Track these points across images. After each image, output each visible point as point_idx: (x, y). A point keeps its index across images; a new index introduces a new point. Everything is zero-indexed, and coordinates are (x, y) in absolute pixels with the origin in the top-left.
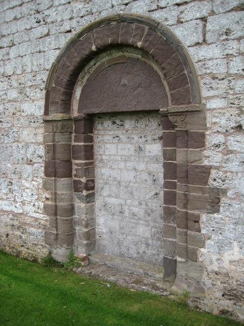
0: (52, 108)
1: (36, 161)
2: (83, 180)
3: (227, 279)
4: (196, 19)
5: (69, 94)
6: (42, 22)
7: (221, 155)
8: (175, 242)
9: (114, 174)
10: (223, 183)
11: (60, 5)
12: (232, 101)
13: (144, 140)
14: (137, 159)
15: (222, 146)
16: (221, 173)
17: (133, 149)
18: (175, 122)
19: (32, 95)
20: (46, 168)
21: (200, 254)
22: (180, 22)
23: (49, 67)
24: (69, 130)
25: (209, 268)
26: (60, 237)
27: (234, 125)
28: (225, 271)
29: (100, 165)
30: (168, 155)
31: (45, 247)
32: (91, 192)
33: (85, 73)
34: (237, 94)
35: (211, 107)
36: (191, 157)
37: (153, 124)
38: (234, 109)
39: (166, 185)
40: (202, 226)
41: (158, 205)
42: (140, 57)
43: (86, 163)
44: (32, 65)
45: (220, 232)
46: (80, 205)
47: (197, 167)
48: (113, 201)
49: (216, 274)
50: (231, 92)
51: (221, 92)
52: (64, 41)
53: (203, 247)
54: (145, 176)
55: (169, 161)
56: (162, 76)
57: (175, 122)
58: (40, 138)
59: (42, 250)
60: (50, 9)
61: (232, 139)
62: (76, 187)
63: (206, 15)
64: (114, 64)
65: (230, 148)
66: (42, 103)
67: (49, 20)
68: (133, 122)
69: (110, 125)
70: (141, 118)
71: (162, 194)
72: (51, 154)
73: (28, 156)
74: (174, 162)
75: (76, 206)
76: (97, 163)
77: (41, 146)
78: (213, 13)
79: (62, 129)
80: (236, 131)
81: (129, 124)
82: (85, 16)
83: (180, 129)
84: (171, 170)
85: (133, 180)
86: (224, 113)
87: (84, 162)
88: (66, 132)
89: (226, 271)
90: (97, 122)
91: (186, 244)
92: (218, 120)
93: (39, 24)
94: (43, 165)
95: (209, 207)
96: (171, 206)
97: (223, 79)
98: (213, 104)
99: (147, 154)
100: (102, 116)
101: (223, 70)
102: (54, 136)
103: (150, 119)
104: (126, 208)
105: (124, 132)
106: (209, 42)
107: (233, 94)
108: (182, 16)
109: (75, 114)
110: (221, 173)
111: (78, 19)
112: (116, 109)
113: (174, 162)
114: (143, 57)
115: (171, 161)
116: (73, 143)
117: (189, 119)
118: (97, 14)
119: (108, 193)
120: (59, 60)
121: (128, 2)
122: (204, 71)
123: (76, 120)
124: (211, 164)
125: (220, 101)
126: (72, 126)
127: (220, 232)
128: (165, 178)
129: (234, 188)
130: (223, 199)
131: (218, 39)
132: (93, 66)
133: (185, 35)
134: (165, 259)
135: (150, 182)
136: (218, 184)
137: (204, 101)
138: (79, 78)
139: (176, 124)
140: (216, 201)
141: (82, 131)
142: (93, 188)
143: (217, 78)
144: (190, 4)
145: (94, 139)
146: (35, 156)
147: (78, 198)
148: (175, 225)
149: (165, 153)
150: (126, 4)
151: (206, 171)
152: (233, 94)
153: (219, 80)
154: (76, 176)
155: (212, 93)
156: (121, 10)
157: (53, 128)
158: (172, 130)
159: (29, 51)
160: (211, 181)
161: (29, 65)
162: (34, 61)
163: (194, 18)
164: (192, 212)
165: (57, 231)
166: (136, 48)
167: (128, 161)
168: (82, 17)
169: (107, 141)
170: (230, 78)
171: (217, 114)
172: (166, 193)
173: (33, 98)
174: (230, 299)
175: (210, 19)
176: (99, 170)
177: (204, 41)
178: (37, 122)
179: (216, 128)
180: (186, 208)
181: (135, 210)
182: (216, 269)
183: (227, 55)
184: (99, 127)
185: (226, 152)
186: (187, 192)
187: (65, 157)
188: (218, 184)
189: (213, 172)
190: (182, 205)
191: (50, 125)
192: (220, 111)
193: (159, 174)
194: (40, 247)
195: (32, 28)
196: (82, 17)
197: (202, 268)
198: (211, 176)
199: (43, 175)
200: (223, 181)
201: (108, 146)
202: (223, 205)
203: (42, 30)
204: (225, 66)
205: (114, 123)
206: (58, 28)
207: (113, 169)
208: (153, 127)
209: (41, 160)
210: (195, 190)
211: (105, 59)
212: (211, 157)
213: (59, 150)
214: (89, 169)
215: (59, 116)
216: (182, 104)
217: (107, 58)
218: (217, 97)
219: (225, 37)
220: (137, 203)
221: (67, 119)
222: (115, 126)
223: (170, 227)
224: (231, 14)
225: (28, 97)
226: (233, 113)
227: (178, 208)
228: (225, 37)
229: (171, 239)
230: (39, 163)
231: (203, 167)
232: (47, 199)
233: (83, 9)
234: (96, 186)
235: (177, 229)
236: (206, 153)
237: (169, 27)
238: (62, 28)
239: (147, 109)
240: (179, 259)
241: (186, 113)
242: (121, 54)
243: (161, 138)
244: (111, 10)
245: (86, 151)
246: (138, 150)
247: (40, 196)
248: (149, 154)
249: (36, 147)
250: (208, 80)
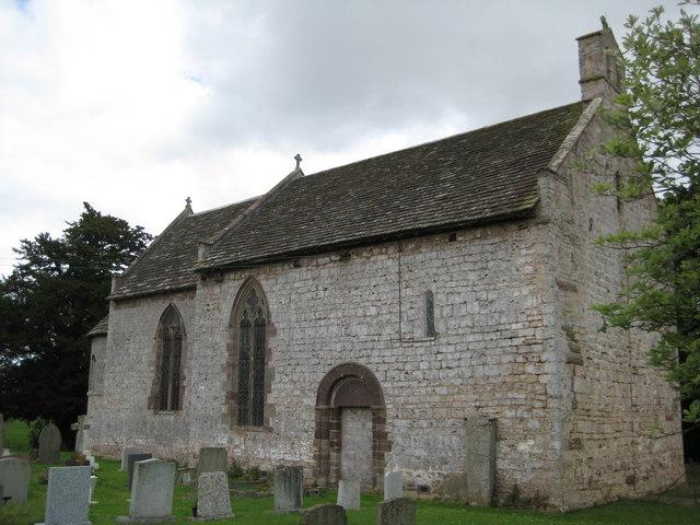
5: (329, 396)
46: (333, 454)
81: (359, 412)
109: (332, 406)
132: (342, 383)
167: (356, 430)
208: (369, 415)
212: (388, 428)
214: (339, 435)
215: (324, 407)
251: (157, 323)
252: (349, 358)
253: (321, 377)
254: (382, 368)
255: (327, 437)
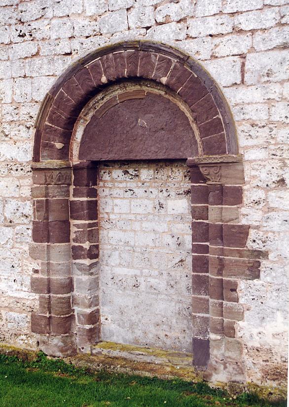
0: (44, 153)
1: (20, 222)
2: (86, 245)
3: (270, 355)
4: (233, 55)
5: (67, 137)
6: (27, 37)
7: (261, 212)
8: (207, 318)
9: (128, 236)
10: (265, 244)
11: (54, 17)
12: (274, 152)
13: (166, 194)
14: (156, 218)
15: (262, 202)
16: (261, 233)
17: (150, 207)
18: (207, 175)
19: (12, 133)
20: (34, 231)
21: (239, 328)
22: (214, 57)
23: (41, 97)
24: (67, 182)
25: (250, 345)
26: (53, 321)
27: (276, 179)
28: (268, 347)
29: (107, 226)
30: (197, 213)
31: (31, 337)
32: (94, 261)
33: (90, 109)
34: (279, 144)
35: (250, 159)
36: (227, 215)
37: (177, 174)
38: (276, 161)
39: (195, 249)
40: (240, 294)
41: (184, 276)
42: (163, 93)
43: (89, 224)
44: (14, 93)
45: (261, 300)
46: (81, 278)
47: (233, 227)
48: (121, 271)
49: (258, 350)
50: (273, 142)
51: (261, 141)
52: (61, 67)
53: (242, 319)
54: (168, 239)
55: (199, 221)
56: (191, 119)
57: (207, 175)
58: (26, 192)
59: (26, 341)
60: (39, 21)
61: (273, 194)
62: (76, 253)
63: (245, 51)
64: (129, 100)
65: (272, 205)
66: (30, 145)
67: (38, 35)
68: (151, 172)
69: (120, 175)
70: (161, 167)
71: (189, 261)
72: (43, 213)
73: (6, 215)
74: (205, 221)
75: (75, 280)
76: (102, 223)
77: (28, 203)
78: (252, 49)
79: (59, 180)
80: (278, 186)
81: (146, 173)
82: (90, 36)
83: (212, 184)
84: (203, 232)
85: (151, 244)
86: (264, 166)
87: (87, 222)
88: (63, 184)
89: (269, 347)
90: (103, 171)
91: (220, 318)
92: (257, 173)
93: (22, 39)
94: (31, 227)
95: (248, 272)
96: (201, 274)
97: (264, 126)
98: (249, 155)
99: (170, 211)
100: (109, 164)
101: (264, 116)
102: (47, 188)
103: (174, 169)
104: (141, 280)
105: (140, 184)
106: (249, 83)
107: (275, 144)
108: (216, 50)
109: (75, 161)
110: (261, 233)
111: (83, 39)
112: (132, 157)
113: (205, 221)
114: (166, 93)
115: (201, 221)
116: (72, 199)
117: (224, 171)
118: (109, 35)
119: (118, 262)
120: (55, 89)
121: (149, 26)
122: (242, 117)
123: (76, 169)
124: (250, 223)
125: (260, 151)
126: (71, 177)
127: (261, 300)
128: (194, 240)
129: (277, 249)
130: (264, 262)
131: (259, 82)
132: (101, 100)
133: (221, 73)
134: (195, 340)
135: (173, 246)
136: (258, 246)
137: (241, 151)
138: (81, 115)
139: (208, 177)
140: (256, 265)
141: (85, 182)
142: (96, 256)
143: (257, 125)
144: (226, 37)
145: (98, 192)
146: (18, 214)
147: (79, 269)
148: (207, 297)
149: (194, 213)
150: (147, 28)
151: (243, 232)
152: (275, 144)
153: (260, 127)
154: (75, 240)
155: (250, 142)
156: (140, 34)
157: (46, 179)
158: (202, 183)
159: (9, 74)
160: (251, 242)
161: (9, 93)
162: (15, 88)
163: (231, 54)
164: (228, 279)
165: (50, 313)
166: (160, 83)
167: (145, 217)
168: (87, 37)
169: (117, 196)
170: (271, 126)
171: (256, 167)
172: (195, 259)
173: (15, 138)
174: (274, 380)
175: (249, 56)
176: (105, 232)
177: (243, 81)
178: (22, 169)
179: (255, 182)
180: (221, 275)
181: (153, 281)
182: (257, 345)
183: (268, 99)
184: (106, 177)
185: (267, 210)
186: (219, 255)
187: (63, 217)
188: (258, 246)
189: (252, 232)
190: (216, 271)
191: (41, 177)
192: (260, 162)
193: (185, 237)
194: (24, 337)
195: (11, 43)
196: (87, 37)
197: (240, 346)
198: (249, 237)
199: (30, 240)
200: (264, 242)
201: (117, 201)
202: (264, 269)
203: (26, 48)
204: (266, 112)
205: (126, 172)
206: (52, 48)
207: (125, 231)
208: (178, 178)
209: (26, 221)
210: (231, 253)
211: (117, 92)
213: (53, 207)
214: (93, 233)
215: (56, 163)
216: (216, 154)
217: (120, 92)
218: (257, 146)
219: (266, 79)
220: (156, 273)
221: (65, 168)
222: (127, 177)
223: (201, 299)
224: (270, 52)
225: (7, 136)
226: (275, 166)
227: (212, 275)
228: (266, 79)
229: (201, 315)
230: (25, 224)
231: (242, 226)
232: (36, 271)
233: (90, 28)
234: (101, 252)
235: (211, 300)
236: (244, 210)
237: (200, 62)
238: (58, 48)
239: (170, 157)
240: (213, 336)
241: (220, 165)
242: (138, 87)
243: (188, 192)
244: (127, 32)
245: (89, 208)
246: (158, 207)
247: (25, 268)
248: (172, 212)
249: (20, 203)
250: (246, 127)
251: (275, 52)
252: (123, 29)
253: (45, 86)
254: (229, 46)
255: (65, 237)
